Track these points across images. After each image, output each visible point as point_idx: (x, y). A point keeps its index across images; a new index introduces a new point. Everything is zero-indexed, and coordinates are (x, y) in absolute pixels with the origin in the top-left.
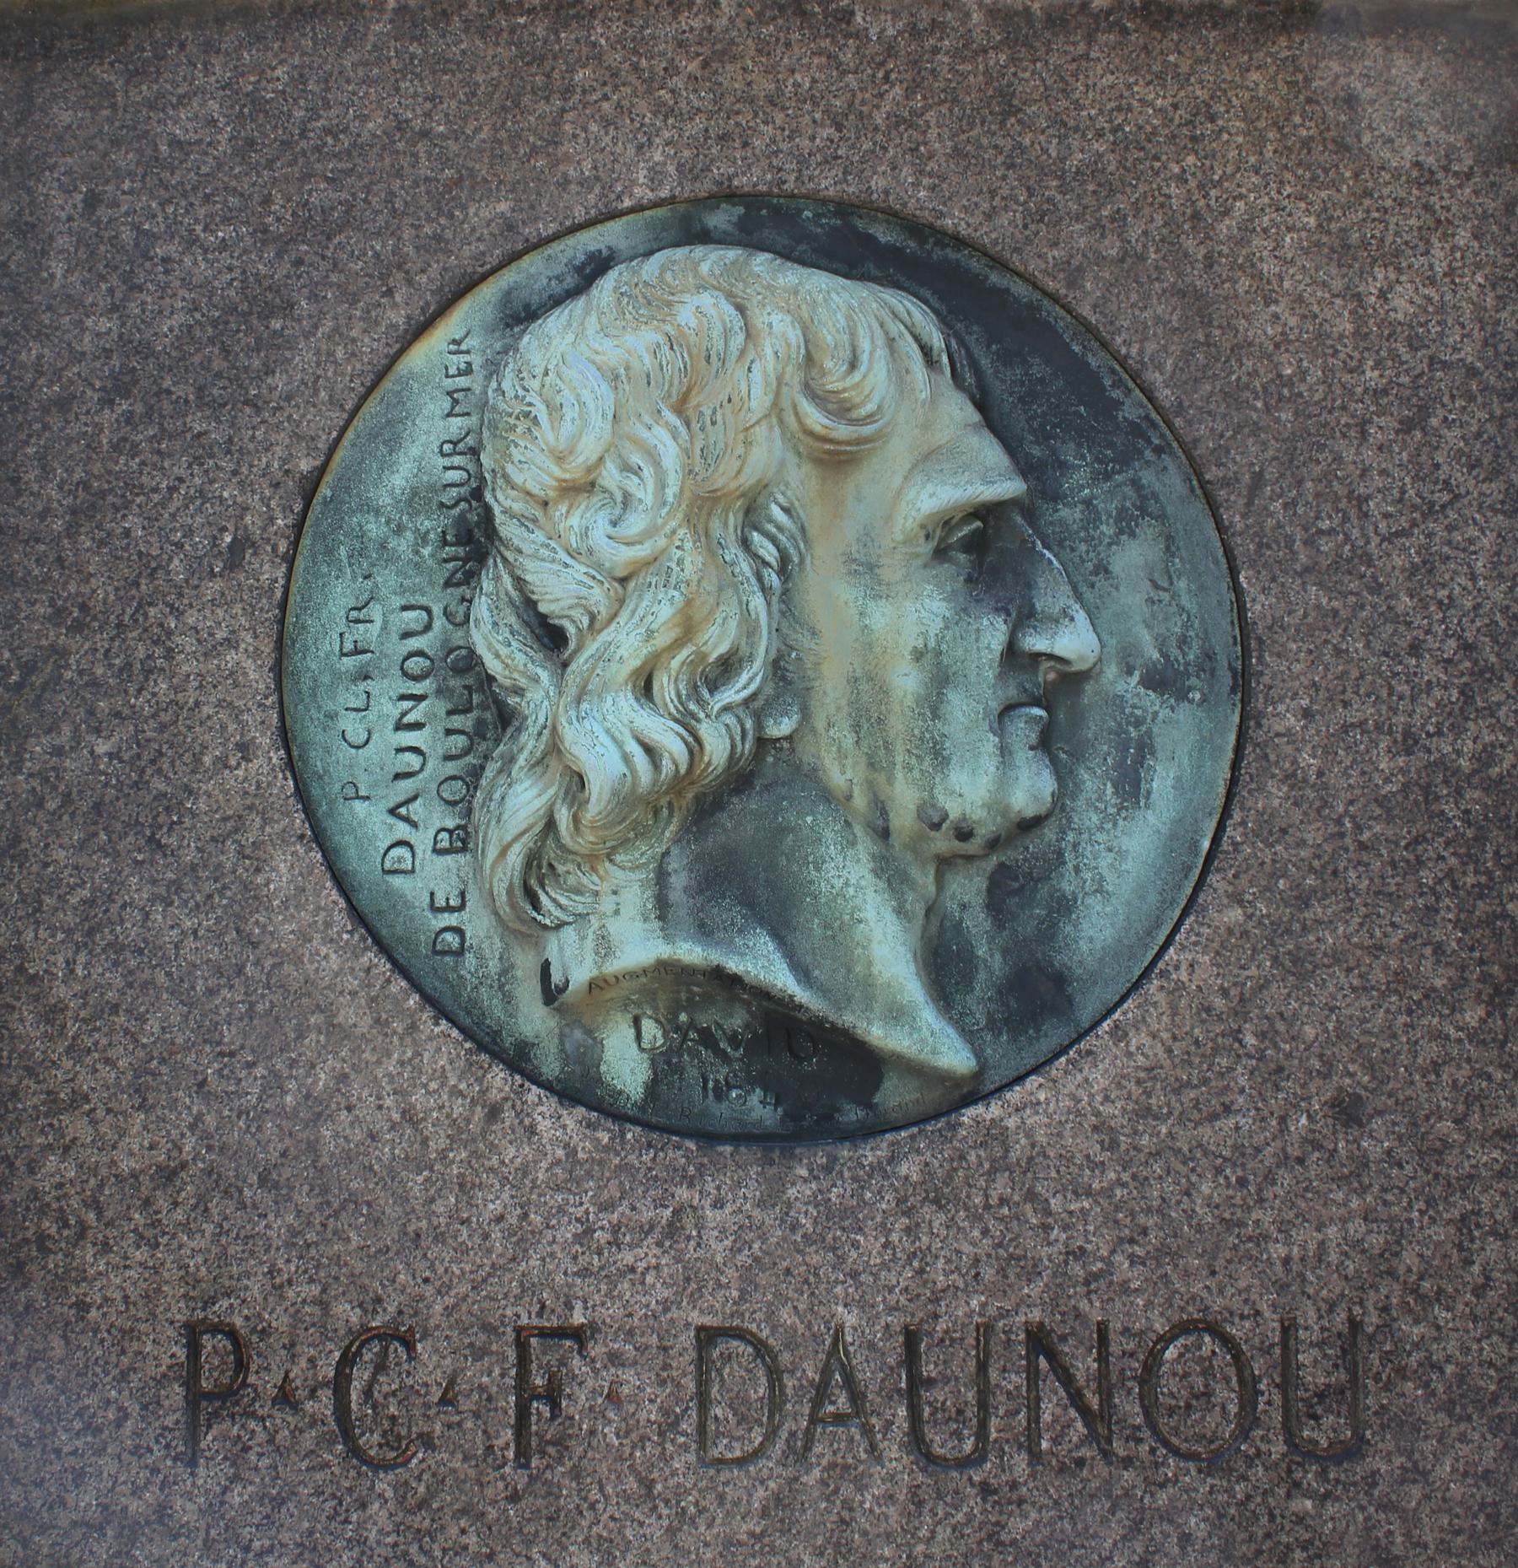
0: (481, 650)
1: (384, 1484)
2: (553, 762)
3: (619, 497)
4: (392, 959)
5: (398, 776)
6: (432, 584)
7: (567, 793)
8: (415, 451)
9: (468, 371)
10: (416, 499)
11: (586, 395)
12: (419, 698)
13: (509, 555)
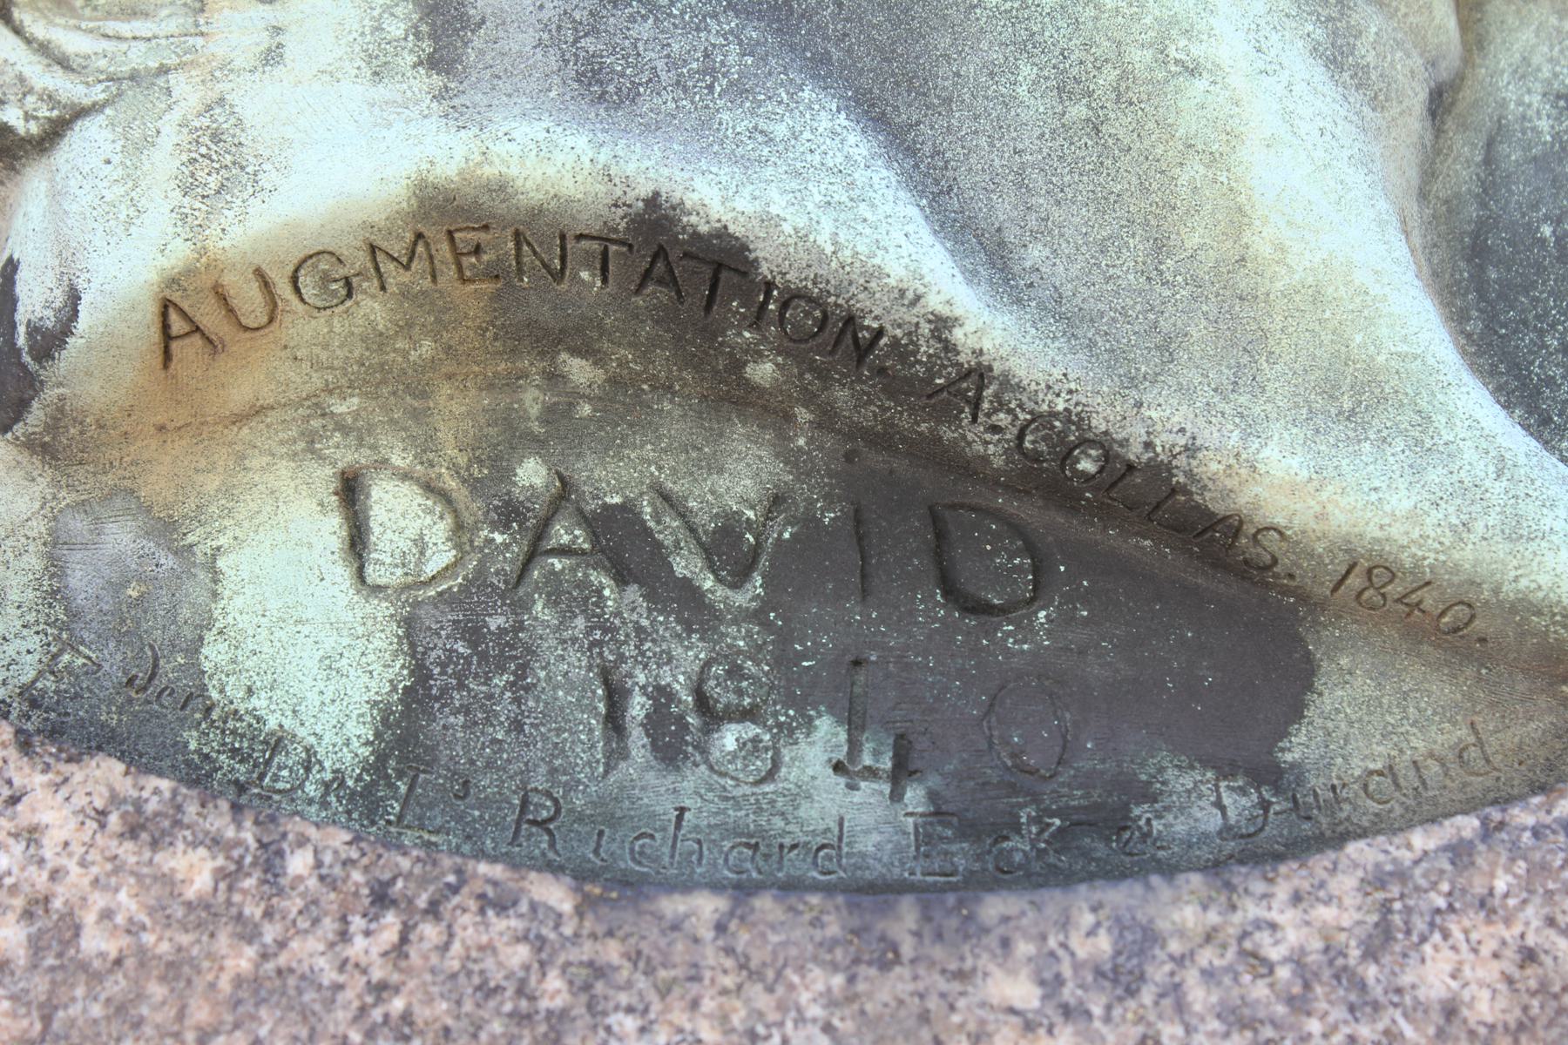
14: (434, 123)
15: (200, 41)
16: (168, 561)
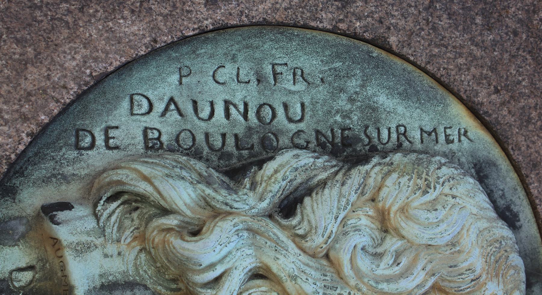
0: (280, 160)
2: (208, 212)
3: (379, 250)
4: (73, 102)
5: (195, 103)
6: (318, 122)
7: (187, 223)
8: (400, 109)
9: (449, 141)
10: (371, 111)
11: (443, 227)
12: (245, 116)
13: (339, 177)
14: (87, 288)
15: (110, 242)
16: (17, 237)
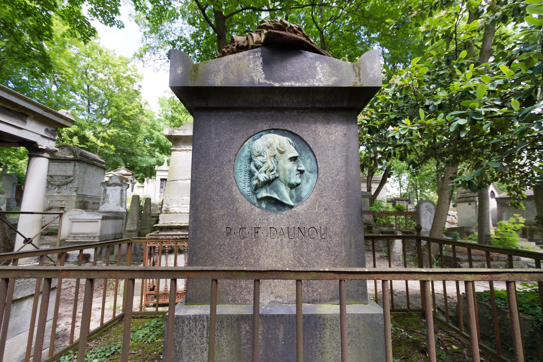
1: (243, 241)
